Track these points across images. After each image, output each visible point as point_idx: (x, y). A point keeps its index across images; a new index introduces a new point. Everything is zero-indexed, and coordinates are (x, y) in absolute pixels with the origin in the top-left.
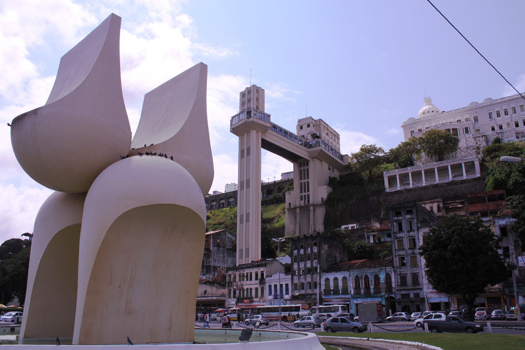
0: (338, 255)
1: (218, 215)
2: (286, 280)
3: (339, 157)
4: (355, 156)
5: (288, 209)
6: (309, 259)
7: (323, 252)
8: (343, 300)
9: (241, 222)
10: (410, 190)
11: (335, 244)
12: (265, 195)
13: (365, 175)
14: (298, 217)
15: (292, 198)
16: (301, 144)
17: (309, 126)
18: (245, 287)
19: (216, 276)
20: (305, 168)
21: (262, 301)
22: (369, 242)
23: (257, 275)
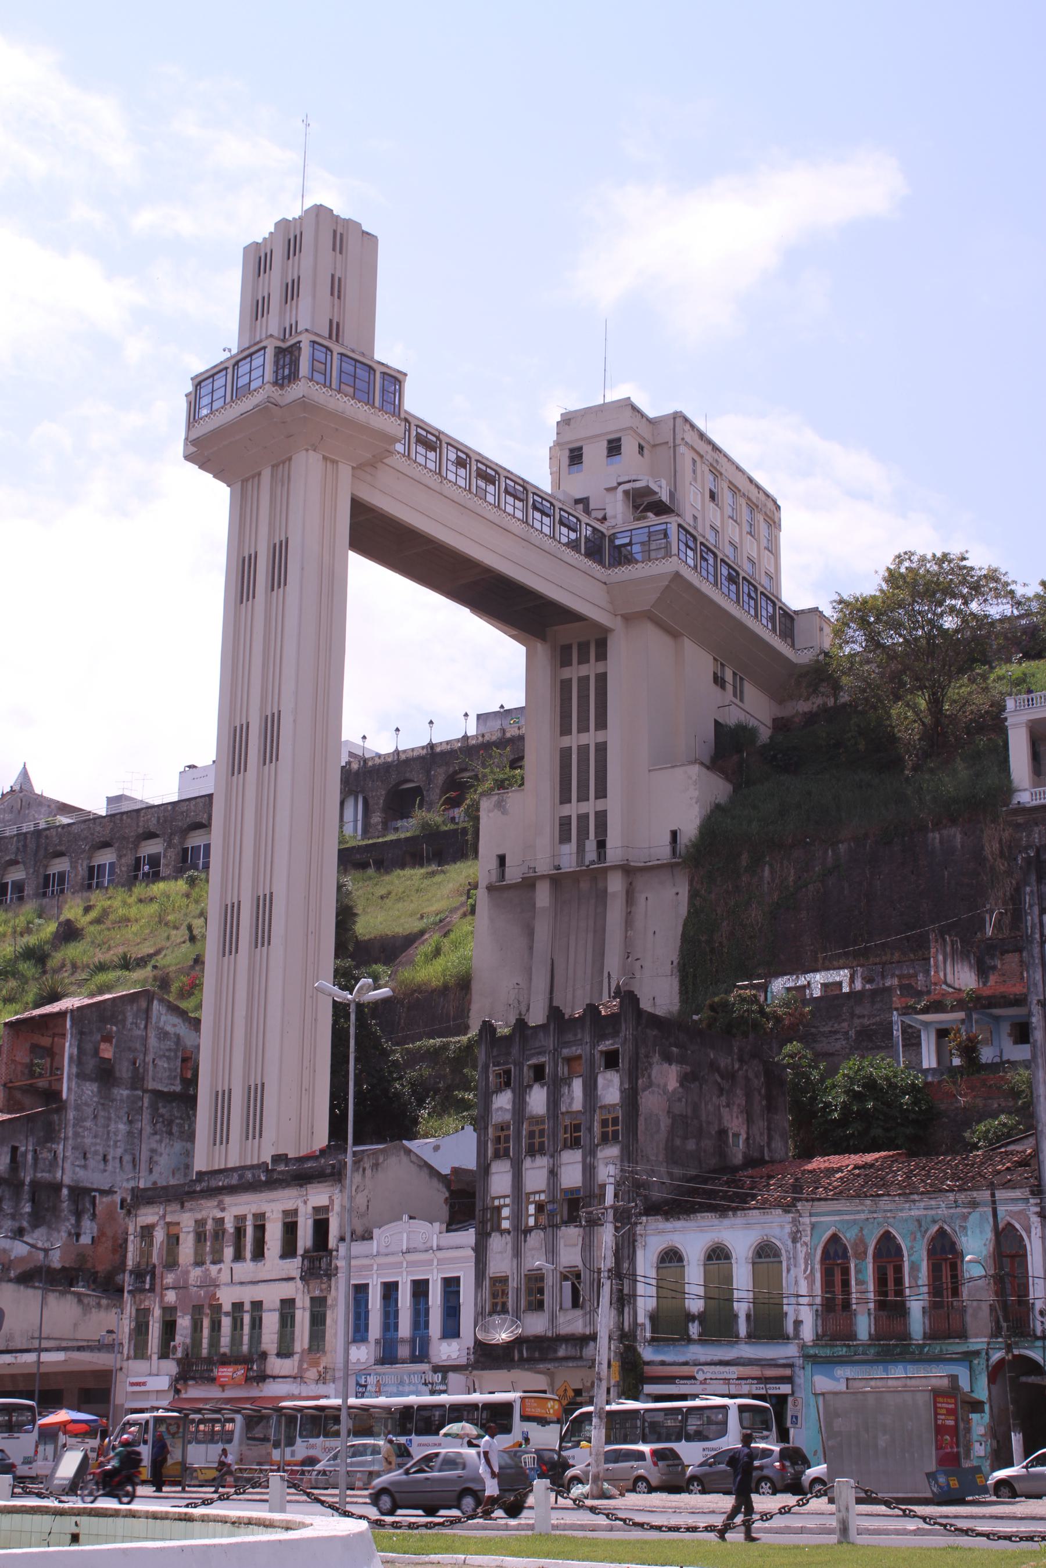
0: (735, 1124)
1: (126, 920)
2: (441, 1254)
3: (772, 618)
4: (858, 612)
5: (490, 888)
6: (575, 1143)
7: (651, 1102)
8: (755, 1371)
9: (229, 945)
11: (724, 1062)
12: (376, 818)
13: (907, 717)
14: (542, 930)
15: (517, 826)
16: (574, 545)
17: (614, 448)
18: (226, 1298)
19: (85, 1240)
20: (590, 670)
21: (312, 1374)
22: (915, 1064)
23: (290, 1229)
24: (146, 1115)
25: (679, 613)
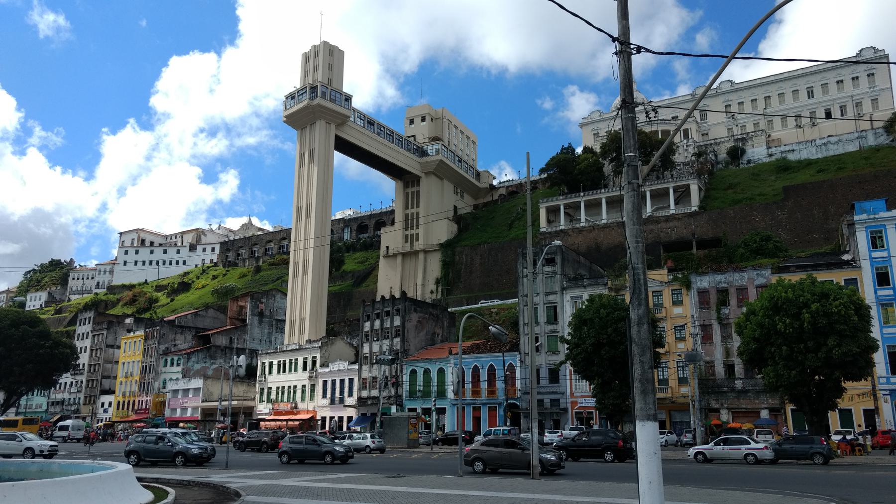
7: (409, 325)
10: (581, 230)
20: (415, 189)
23: (305, 363)
24: (274, 327)
25: (441, 171)
